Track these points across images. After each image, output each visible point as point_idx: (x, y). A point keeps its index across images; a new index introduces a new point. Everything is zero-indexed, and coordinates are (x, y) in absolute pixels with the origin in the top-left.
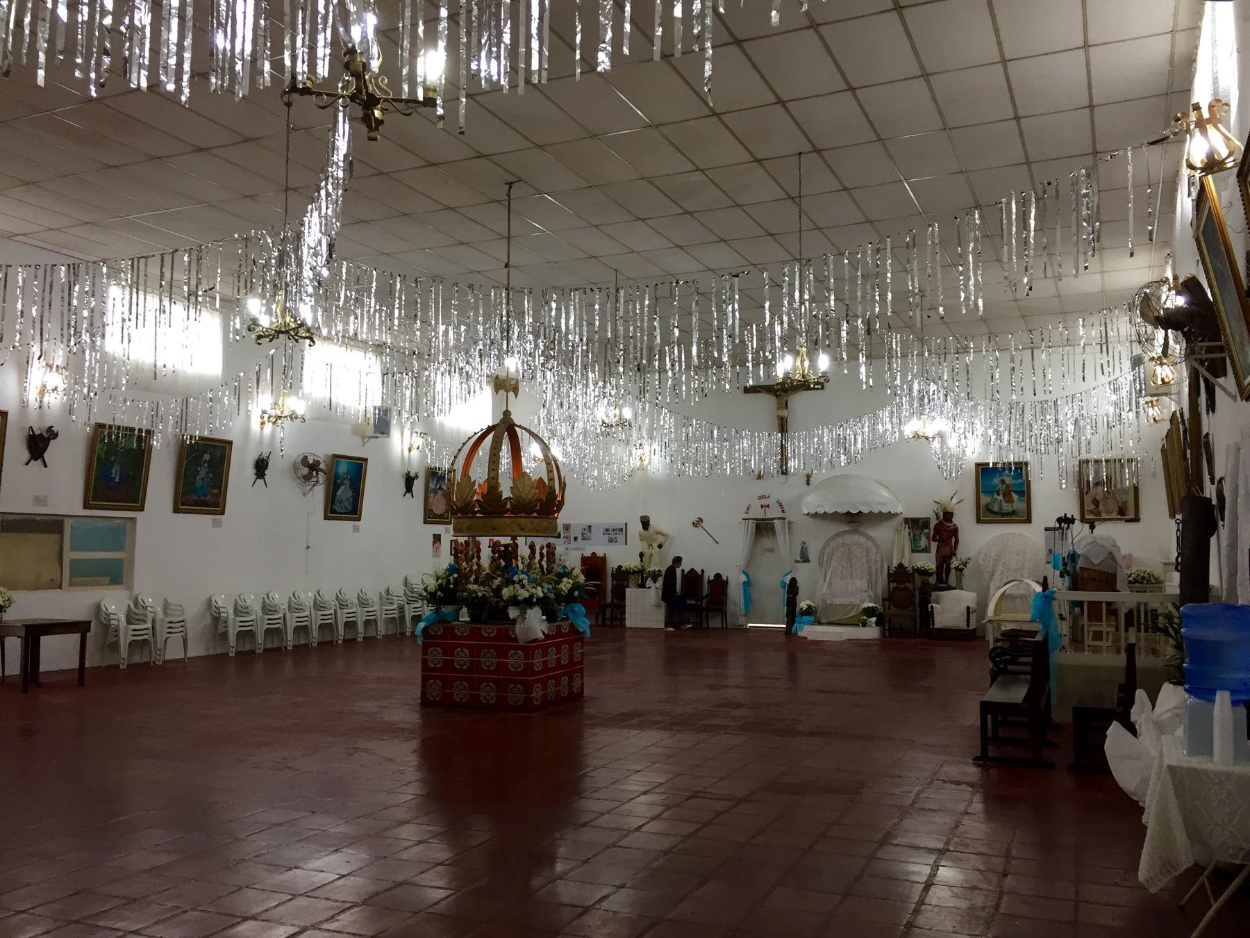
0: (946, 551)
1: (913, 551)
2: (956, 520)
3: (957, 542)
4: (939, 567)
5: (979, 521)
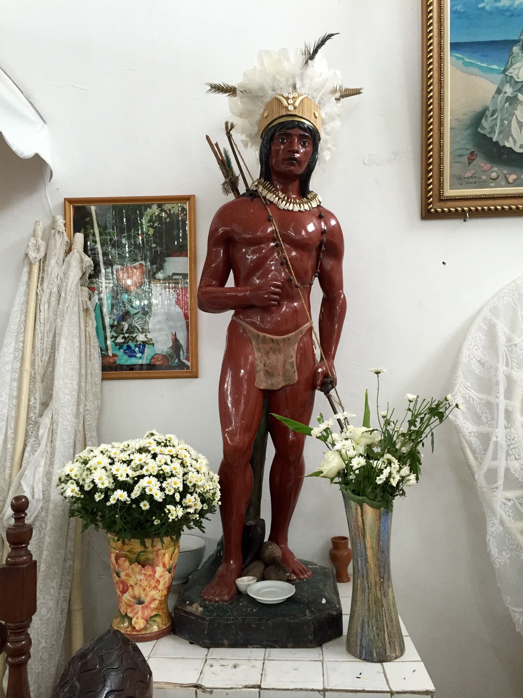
0: (274, 366)
1: (111, 369)
2: (328, 186)
3: (334, 310)
4: (237, 469)
5: (434, 207)
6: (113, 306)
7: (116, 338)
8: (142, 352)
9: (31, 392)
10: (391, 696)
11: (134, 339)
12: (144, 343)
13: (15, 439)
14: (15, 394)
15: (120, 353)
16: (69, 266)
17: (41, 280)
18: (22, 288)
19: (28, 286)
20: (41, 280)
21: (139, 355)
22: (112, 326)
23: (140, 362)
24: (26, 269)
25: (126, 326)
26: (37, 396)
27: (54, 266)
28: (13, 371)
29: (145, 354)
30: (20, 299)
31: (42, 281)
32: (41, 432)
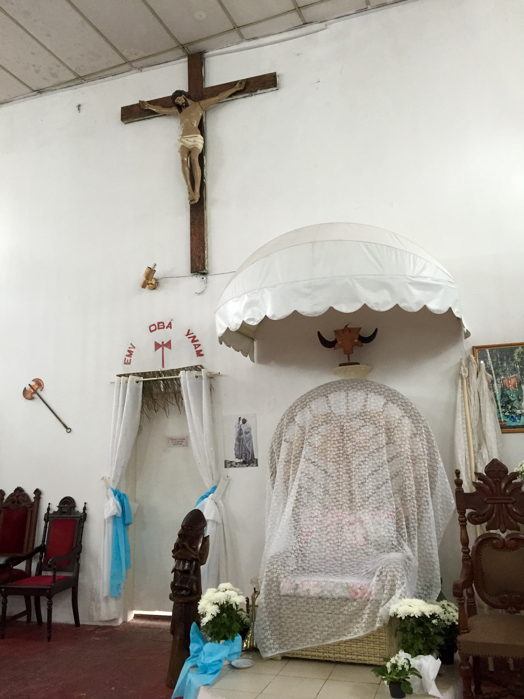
6: (502, 397)
7: (505, 412)
8: (520, 419)
9: (473, 439)
10: (296, 4)
11: (514, 413)
12: (520, 415)
13: (470, 459)
14: (466, 439)
15: (508, 420)
16: (481, 378)
17: (469, 386)
18: (460, 390)
19: (463, 389)
20: (469, 386)
21: (518, 421)
22: (502, 407)
23: (519, 424)
24: (460, 381)
25: (510, 407)
26: (476, 440)
27: (474, 379)
28: (463, 429)
29: (522, 420)
30: (459, 396)
31: (469, 387)
32: (484, 456)
